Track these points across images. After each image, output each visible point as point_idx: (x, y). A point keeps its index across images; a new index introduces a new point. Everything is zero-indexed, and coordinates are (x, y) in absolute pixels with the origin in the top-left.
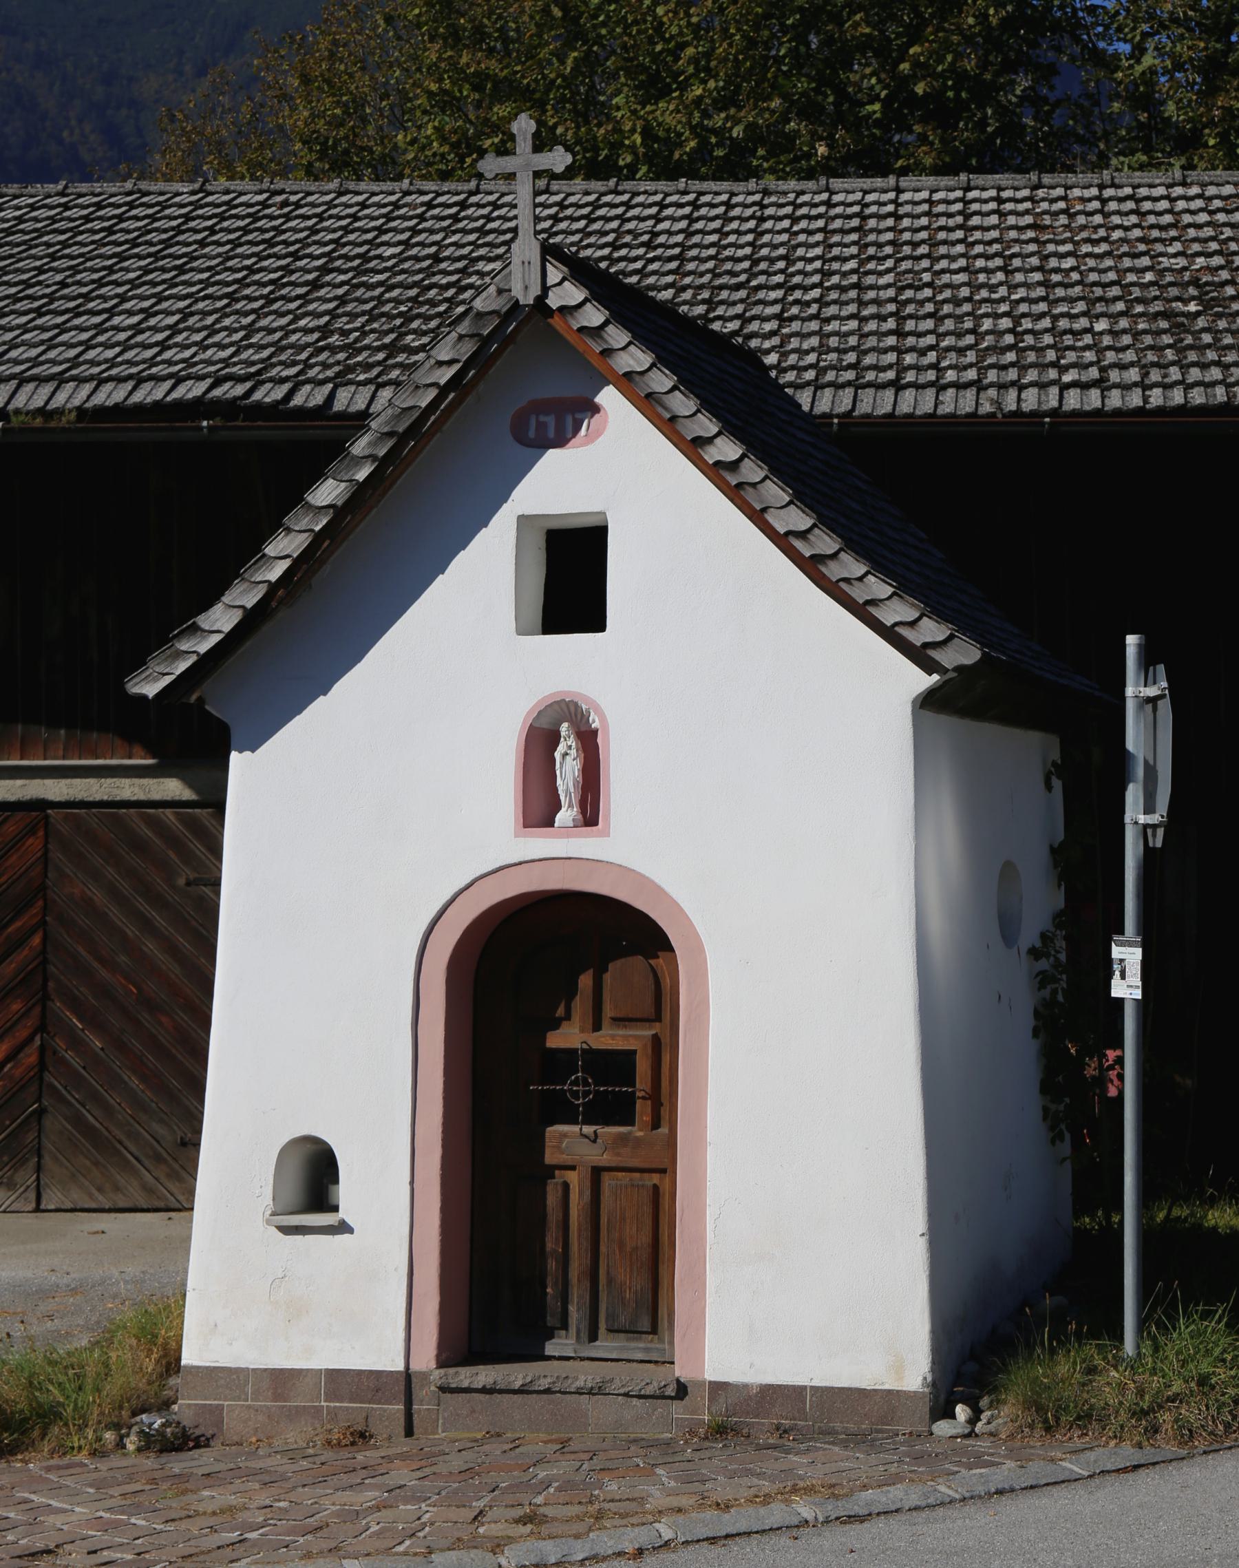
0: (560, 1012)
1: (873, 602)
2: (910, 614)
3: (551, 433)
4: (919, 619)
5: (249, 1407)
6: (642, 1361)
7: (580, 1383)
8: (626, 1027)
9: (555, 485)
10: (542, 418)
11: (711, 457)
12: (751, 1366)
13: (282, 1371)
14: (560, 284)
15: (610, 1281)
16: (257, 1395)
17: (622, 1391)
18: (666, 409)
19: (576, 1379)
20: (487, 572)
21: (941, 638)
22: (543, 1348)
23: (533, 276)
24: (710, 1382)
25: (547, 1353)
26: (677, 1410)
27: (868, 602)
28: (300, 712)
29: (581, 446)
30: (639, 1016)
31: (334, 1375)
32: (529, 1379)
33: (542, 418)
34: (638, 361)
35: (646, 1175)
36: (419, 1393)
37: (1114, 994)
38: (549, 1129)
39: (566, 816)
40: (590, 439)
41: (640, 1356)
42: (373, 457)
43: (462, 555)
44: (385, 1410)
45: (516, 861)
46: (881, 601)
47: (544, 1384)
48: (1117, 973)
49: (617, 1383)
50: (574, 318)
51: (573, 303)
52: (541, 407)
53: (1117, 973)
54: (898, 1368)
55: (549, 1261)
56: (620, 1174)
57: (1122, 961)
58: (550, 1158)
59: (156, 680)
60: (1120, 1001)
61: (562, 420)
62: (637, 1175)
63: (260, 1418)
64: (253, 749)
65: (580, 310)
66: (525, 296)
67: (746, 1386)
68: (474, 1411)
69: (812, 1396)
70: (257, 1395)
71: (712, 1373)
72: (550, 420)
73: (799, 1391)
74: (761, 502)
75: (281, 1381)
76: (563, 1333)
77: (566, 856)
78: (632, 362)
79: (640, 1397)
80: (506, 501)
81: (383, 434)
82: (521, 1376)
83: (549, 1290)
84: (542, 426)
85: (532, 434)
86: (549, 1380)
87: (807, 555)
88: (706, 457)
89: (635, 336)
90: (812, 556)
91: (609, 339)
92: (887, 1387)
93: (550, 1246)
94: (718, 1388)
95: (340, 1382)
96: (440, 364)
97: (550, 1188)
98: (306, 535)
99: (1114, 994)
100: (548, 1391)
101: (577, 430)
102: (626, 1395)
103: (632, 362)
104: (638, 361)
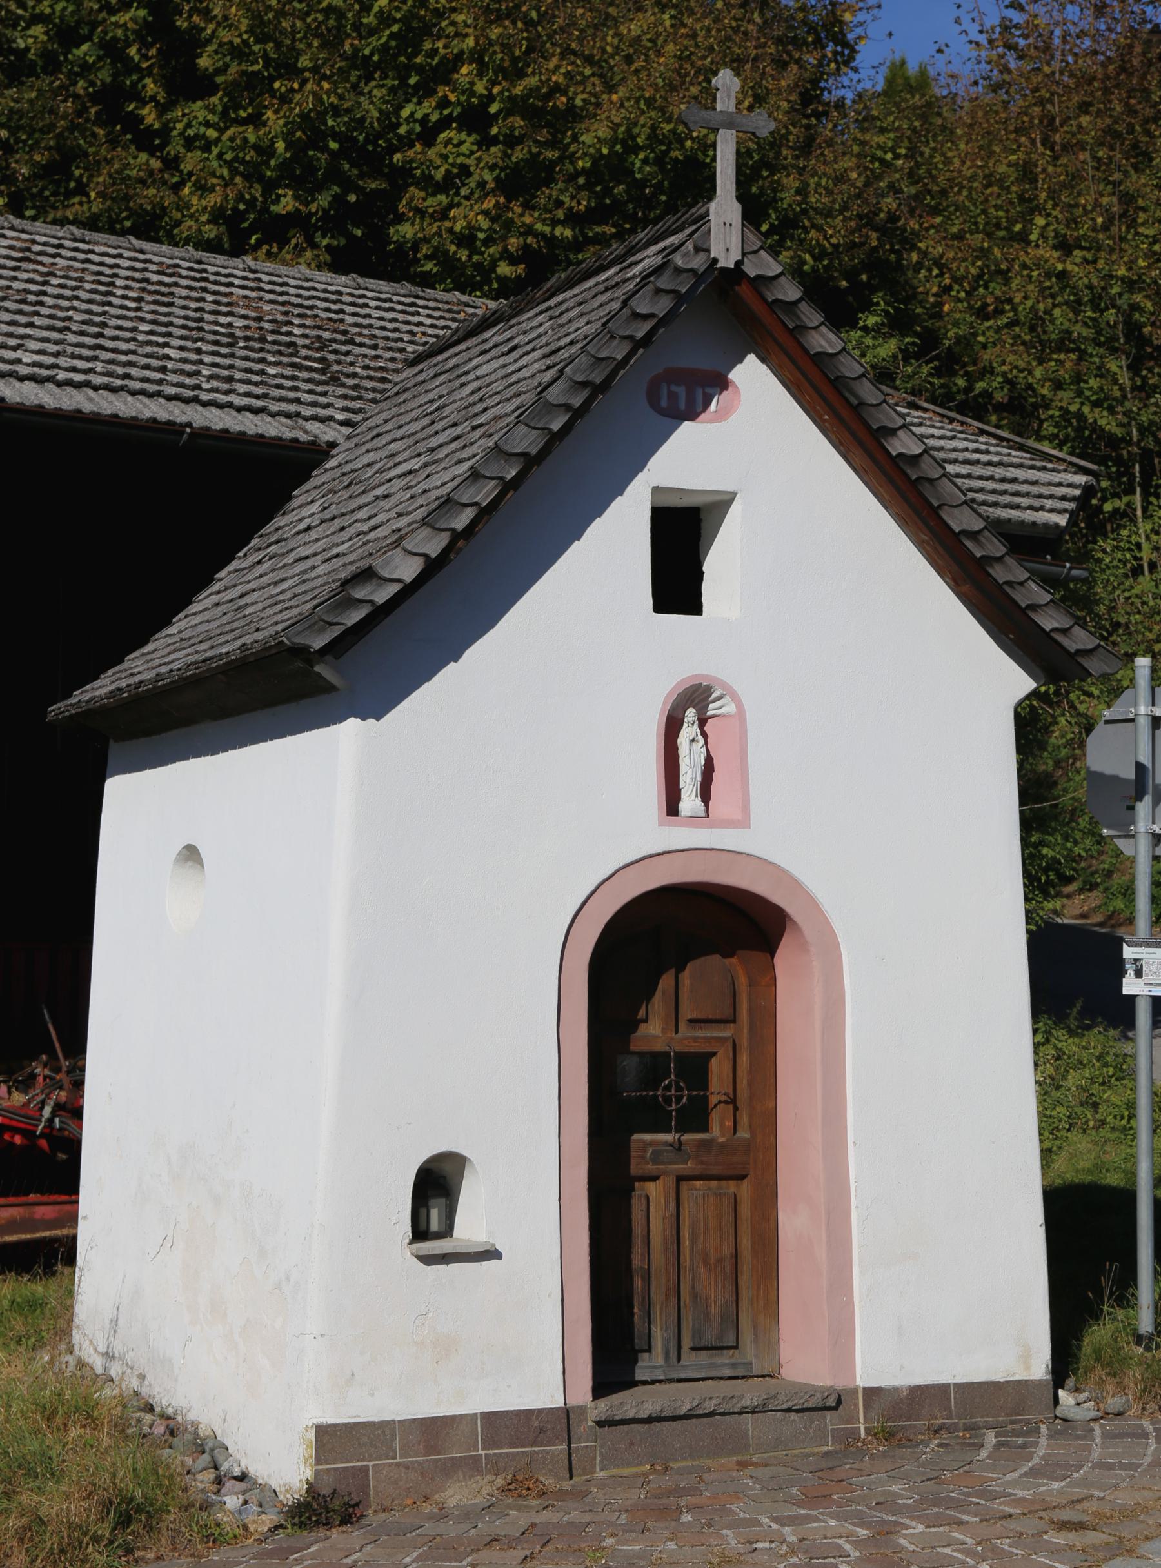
0: (642, 1014)
1: (1034, 607)
2: (1066, 622)
3: (682, 405)
4: (1072, 627)
5: (398, 1465)
6: (730, 1378)
7: (746, 1402)
8: (701, 1028)
9: (685, 460)
10: (674, 388)
11: (894, 448)
12: (902, 1367)
13: (434, 1420)
14: (756, 252)
15: (695, 1296)
16: (406, 1450)
17: (785, 1406)
18: (856, 396)
19: (741, 1397)
20: (618, 540)
21: (1090, 647)
22: (634, 1373)
23: (734, 239)
24: (864, 1389)
25: (637, 1378)
26: (831, 1421)
27: (1029, 607)
28: (429, 679)
29: (711, 421)
30: (718, 1017)
31: (490, 1418)
32: (695, 1404)
33: (674, 388)
34: (829, 342)
35: (724, 1183)
36: (578, 1430)
37: (1125, 992)
38: (636, 1137)
39: (690, 802)
40: (721, 416)
41: (728, 1372)
42: (567, 407)
43: (598, 522)
44: (548, 1452)
45: (661, 851)
46: (1040, 606)
47: (710, 1406)
48: (1131, 973)
49: (782, 1398)
50: (769, 290)
51: (771, 274)
52: (674, 376)
53: (1131, 973)
54: (1026, 1359)
55: (635, 1279)
56: (698, 1183)
57: (1136, 961)
58: (635, 1169)
59: (322, 630)
60: (1132, 998)
61: (691, 392)
62: (714, 1184)
63: (413, 1475)
64: (378, 718)
65: (775, 282)
66: (727, 259)
67: (896, 1389)
68: (632, 1444)
69: (955, 1393)
70: (406, 1450)
71: (863, 1378)
72: (681, 391)
73: (943, 1389)
74: (938, 499)
75: (432, 1431)
76: (646, 1355)
77: (693, 847)
78: (823, 343)
79: (797, 1411)
80: (641, 471)
81: (577, 383)
82: (687, 1401)
83: (636, 1310)
84: (673, 396)
85: (664, 403)
86: (714, 1402)
87: (978, 555)
88: (889, 448)
89: (826, 319)
90: (982, 557)
91: (802, 316)
92: (1017, 1377)
93: (635, 1263)
94: (872, 1393)
95: (499, 1426)
96: (636, 316)
97: (634, 1201)
98: (493, 482)
99: (1125, 992)
100: (712, 1414)
101: (707, 404)
102: (789, 1410)
103: (823, 343)
104: (829, 342)
